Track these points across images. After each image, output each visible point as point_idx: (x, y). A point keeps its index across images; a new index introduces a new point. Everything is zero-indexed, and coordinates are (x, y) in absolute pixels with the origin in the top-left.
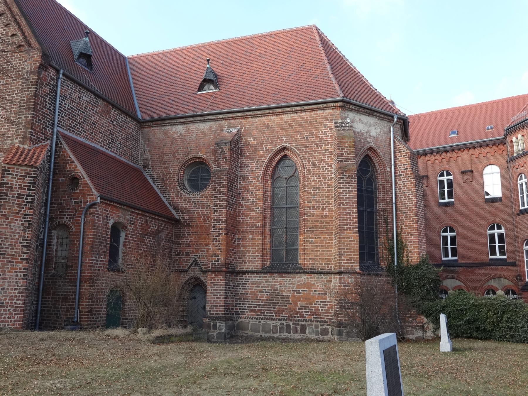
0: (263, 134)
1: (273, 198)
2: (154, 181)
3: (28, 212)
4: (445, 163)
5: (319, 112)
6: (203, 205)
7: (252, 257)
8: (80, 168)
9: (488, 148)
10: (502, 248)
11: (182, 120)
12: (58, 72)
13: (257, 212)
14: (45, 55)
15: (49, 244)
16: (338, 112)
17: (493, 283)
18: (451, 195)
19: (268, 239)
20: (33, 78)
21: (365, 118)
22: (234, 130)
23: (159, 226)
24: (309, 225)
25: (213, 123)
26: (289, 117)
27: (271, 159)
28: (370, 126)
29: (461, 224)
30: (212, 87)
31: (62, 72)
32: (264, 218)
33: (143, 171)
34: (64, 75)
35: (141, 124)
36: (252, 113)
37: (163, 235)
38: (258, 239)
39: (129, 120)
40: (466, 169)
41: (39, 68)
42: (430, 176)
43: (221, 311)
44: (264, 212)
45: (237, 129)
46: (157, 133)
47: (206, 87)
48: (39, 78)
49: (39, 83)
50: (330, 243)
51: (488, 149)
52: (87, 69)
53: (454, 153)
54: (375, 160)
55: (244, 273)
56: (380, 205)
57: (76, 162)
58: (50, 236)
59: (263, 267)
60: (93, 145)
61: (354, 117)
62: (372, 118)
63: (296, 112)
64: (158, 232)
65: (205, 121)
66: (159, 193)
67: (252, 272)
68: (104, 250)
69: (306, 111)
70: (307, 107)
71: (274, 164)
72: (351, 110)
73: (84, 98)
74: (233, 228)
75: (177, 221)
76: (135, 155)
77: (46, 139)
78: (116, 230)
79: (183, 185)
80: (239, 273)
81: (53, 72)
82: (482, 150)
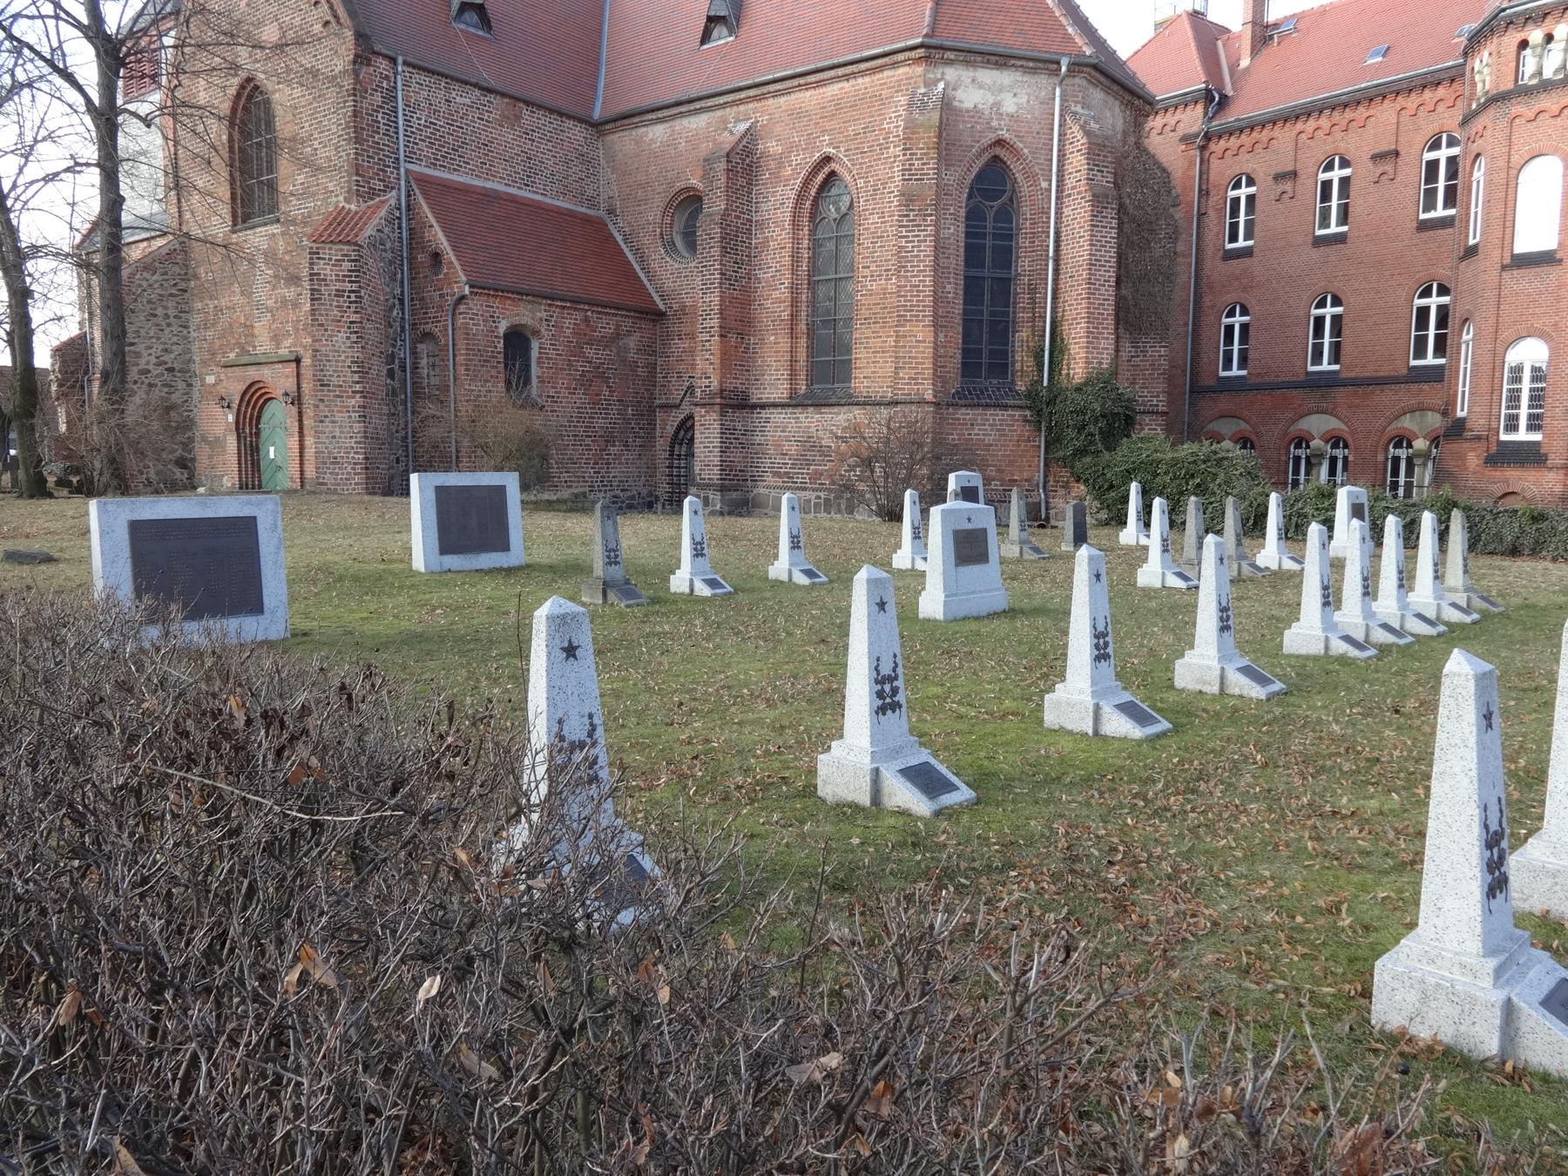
0: (793, 130)
1: (813, 260)
2: (625, 240)
3: (354, 317)
4: (1339, 135)
5: (886, 73)
6: (689, 282)
7: (773, 382)
8: (440, 235)
9: (1440, 88)
10: (1336, 349)
11: (660, 114)
12: (393, 61)
13: (782, 292)
14: (361, 37)
15: (415, 367)
16: (919, 69)
17: (1407, 423)
18: (1344, 218)
19: (803, 342)
20: (348, 83)
21: (988, 76)
22: (743, 127)
23: (618, 326)
24: (865, 313)
26: (833, 90)
27: (806, 183)
28: (1001, 91)
29: (1356, 285)
30: (725, 31)
31: (400, 60)
32: (795, 302)
33: (608, 221)
34: (405, 63)
35: (599, 127)
36: (772, 88)
37: (632, 342)
38: (784, 343)
39: (570, 123)
40: (1385, 147)
41: (355, 62)
42: (1300, 173)
43: (714, 474)
44: (794, 290)
45: (748, 124)
46: (624, 142)
47: (715, 34)
48: (357, 81)
49: (359, 90)
50: (898, 349)
51: (1441, 91)
52: (480, 33)
53: (1361, 109)
54: (1016, 168)
55: (763, 407)
56: (1023, 264)
57: (437, 227)
58: (414, 353)
59: (793, 393)
60: (489, 185)
61: (959, 77)
62: (1006, 73)
63: (847, 77)
64: (617, 336)
67: (775, 405)
68: (494, 372)
69: (862, 73)
71: (813, 192)
72: (950, 62)
73: (458, 99)
74: (739, 323)
75: (662, 314)
76: (590, 192)
77: (388, 187)
78: (517, 341)
80: (754, 407)
81: (383, 65)
82: (1427, 94)
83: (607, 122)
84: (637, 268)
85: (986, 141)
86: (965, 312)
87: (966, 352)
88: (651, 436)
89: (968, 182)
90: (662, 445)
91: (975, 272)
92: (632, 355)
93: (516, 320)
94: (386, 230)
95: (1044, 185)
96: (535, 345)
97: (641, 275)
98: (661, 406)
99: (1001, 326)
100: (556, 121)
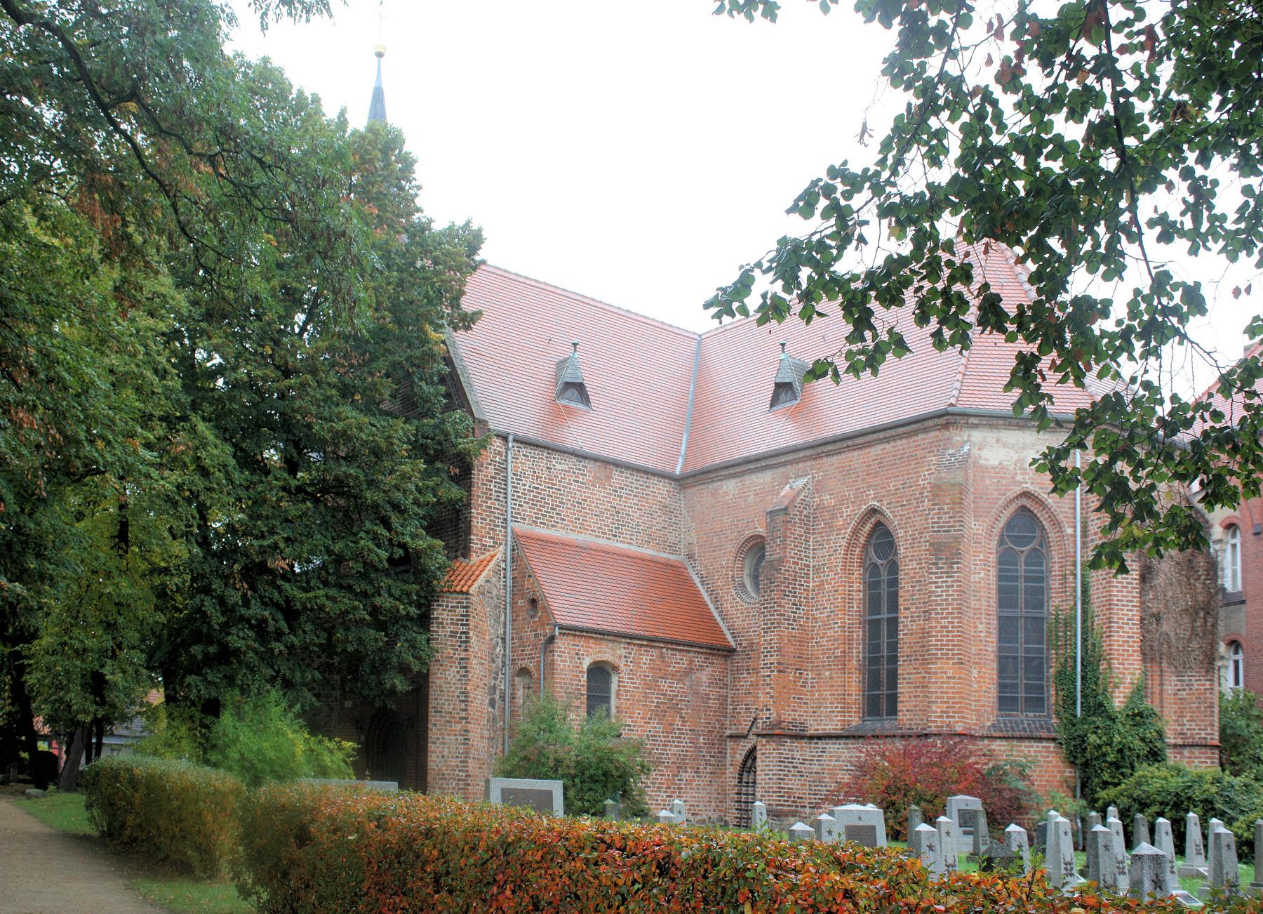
2: (702, 582)
11: (732, 471)
23: (691, 662)
25: (776, 471)
26: (876, 450)
27: (855, 532)
28: (1024, 449)
31: (511, 438)
33: (687, 564)
34: (515, 440)
37: (704, 676)
39: (654, 480)
64: (690, 670)
65: (763, 469)
66: (709, 602)
69: (900, 437)
70: (900, 430)
72: (975, 426)
73: (558, 466)
76: (672, 539)
78: (600, 673)
79: (743, 585)
83: (688, 478)
84: (711, 606)
85: (1011, 495)
86: (1000, 649)
87: (1002, 687)
88: (721, 764)
89: (997, 530)
90: (731, 772)
91: (1009, 613)
92: (704, 688)
93: (599, 657)
94: (494, 580)
95: (1070, 531)
96: (615, 679)
97: (716, 614)
98: (731, 736)
99: (1035, 662)
100: (643, 480)
